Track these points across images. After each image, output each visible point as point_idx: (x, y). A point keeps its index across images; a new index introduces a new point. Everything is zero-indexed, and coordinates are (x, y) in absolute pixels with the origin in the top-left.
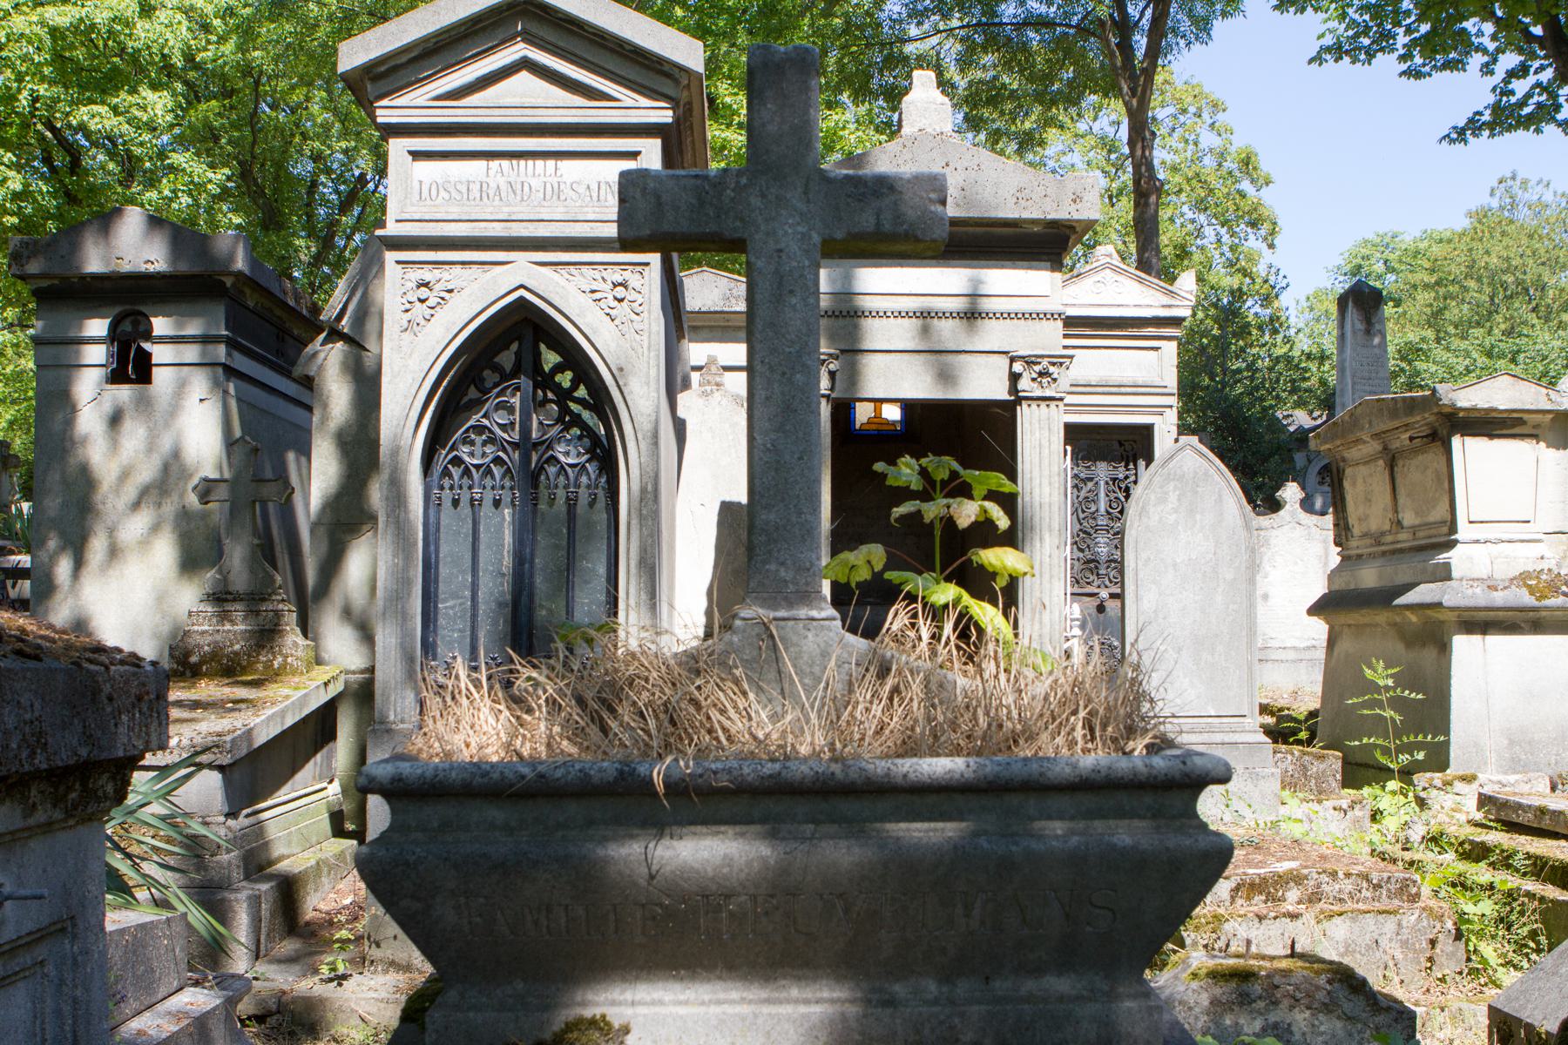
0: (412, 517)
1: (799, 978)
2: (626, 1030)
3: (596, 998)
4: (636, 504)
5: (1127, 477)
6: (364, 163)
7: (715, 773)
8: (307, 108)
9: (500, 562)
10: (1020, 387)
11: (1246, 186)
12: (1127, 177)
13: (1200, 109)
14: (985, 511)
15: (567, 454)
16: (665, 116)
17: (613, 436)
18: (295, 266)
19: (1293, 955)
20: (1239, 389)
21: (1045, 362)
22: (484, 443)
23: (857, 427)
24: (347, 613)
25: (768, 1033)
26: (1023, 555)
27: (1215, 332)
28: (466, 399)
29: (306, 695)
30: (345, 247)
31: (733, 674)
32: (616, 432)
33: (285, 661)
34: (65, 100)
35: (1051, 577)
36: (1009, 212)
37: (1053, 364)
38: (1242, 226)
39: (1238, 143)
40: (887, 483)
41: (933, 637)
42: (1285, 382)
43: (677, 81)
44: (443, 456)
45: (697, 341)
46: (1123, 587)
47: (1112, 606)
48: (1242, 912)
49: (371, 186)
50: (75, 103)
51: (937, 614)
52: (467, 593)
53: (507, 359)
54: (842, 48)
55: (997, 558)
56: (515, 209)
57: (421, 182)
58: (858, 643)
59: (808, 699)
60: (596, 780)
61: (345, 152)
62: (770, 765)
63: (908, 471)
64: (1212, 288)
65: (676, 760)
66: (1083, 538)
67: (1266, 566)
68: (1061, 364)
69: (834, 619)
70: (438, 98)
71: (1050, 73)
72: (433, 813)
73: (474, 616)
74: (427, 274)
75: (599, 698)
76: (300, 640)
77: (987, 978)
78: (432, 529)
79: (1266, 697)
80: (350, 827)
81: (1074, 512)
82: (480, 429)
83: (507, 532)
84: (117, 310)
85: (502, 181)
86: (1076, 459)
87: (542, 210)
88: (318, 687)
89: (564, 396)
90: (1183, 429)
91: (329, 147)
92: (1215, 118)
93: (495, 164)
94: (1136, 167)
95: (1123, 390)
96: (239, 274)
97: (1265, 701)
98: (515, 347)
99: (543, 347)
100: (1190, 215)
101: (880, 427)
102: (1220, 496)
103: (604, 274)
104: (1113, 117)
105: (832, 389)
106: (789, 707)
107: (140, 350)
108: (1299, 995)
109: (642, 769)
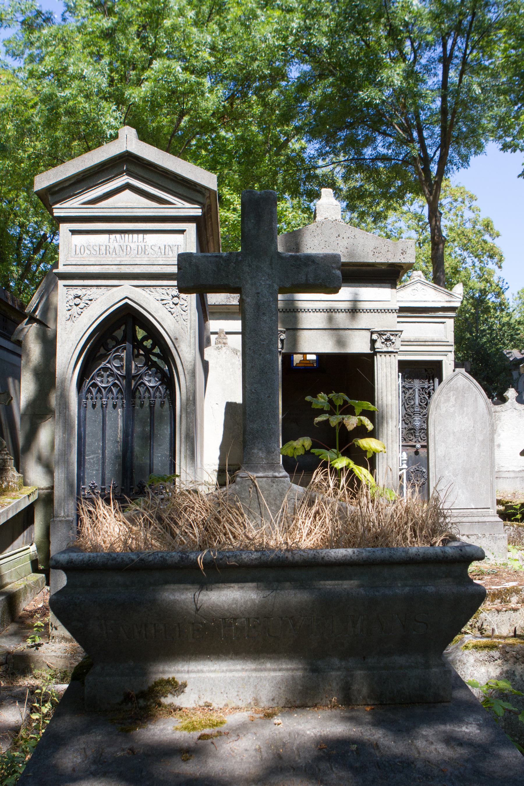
0: (72, 413)
1: (270, 658)
2: (185, 685)
3: (170, 669)
4: (184, 406)
5: (429, 387)
6: (46, 229)
7: (228, 558)
8: (17, 201)
9: (117, 435)
10: (376, 347)
11: (487, 237)
12: (428, 233)
13: (464, 199)
14: (361, 421)
15: (149, 381)
16: (198, 212)
17: (173, 372)
19: (515, 636)
20: (484, 340)
21: (388, 334)
22: (108, 376)
23: (295, 365)
24: (39, 459)
25: (256, 686)
26: (380, 442)
27: (473, 311)
28: (98, 354)
29: (19, 502)
30: (36, 270)
31: (236, 505)
32: (174, 371)
33: (8, 484)
35: (392, 441)
36: (371, 260)
37: (393, 335)
38: (485, 257)
39: (483, 216)
40: (313, 407)
41: (335, 485)
42: (508, 335)
43: (203, 195)
44: (88, 383)
45: (213, 320)
46: (428, 442)
47: (422, 451)
48: (489, 608)
49: (49, 240)
51: (337, 473)
52: (100, 451)
53: (119, 333)
54: (285, 171)
55: (366, 443)
56: (123, 259)
57: (76, 246)
58: (299, 489)
59: (274, 517)
60: (169, 562)
61: (36, 223)
62: (255, 553)
63: (323, 400)
64: (471, 288)
65: (209, 551)
66: (407, 418)
67: (499, 431)
68: (396, 335)
69: (286, 477)
70: (84, 203)
71: (389, 183)
73: (104, 463)
74: (79, 292)
75: (170, 517)
76: (16, 474)
77: (364, 658)
78: (82, 419)
79: (500, 496)
80: (41, 567)
81: (403, 405)
82: (105, 369)
83: (119, 420)
85: (116, 245)
86: (403, 378)
87: (136, 259)
88: (25, 497)
89: (148, 352)
90: (457, 366)
91: (28, 220)
92: (471, 204)
93: (113, 236)
94: (432, 231)
95: (427, 343)
97: (499, 498)
98: (123, 327)
99: (137, 327)
100: (459, 252)
101: (306, 365)
102: (476, 398)
103: (168, 291)
104: (421, 203)
105: (282, 348)
106: (264, 521)
108: (518, 656)
109: (192, 556)
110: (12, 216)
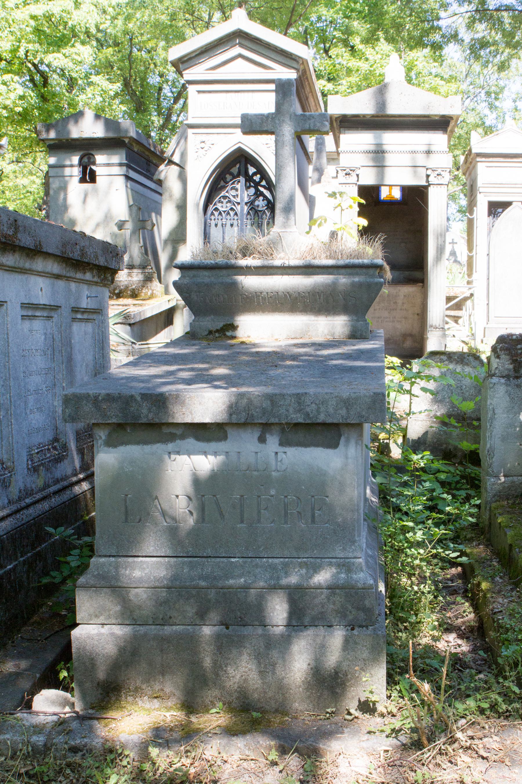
18: (152, 130)
22: (227, 203)
30: (177, 120)
34: (41, 51)
43: (297, 62)
44: (211, 208)
50: (46, 52)
53: (235, 170)
70: (207, 70)
72: (192, 273)
76: (158, 284)
82: (225, 197)
84: (81, 153)
95: (517, 186)
96: (131, 138)
98: (238, 166)
99: (249, 166)
107: (91, 169)
110: (152, 66)
